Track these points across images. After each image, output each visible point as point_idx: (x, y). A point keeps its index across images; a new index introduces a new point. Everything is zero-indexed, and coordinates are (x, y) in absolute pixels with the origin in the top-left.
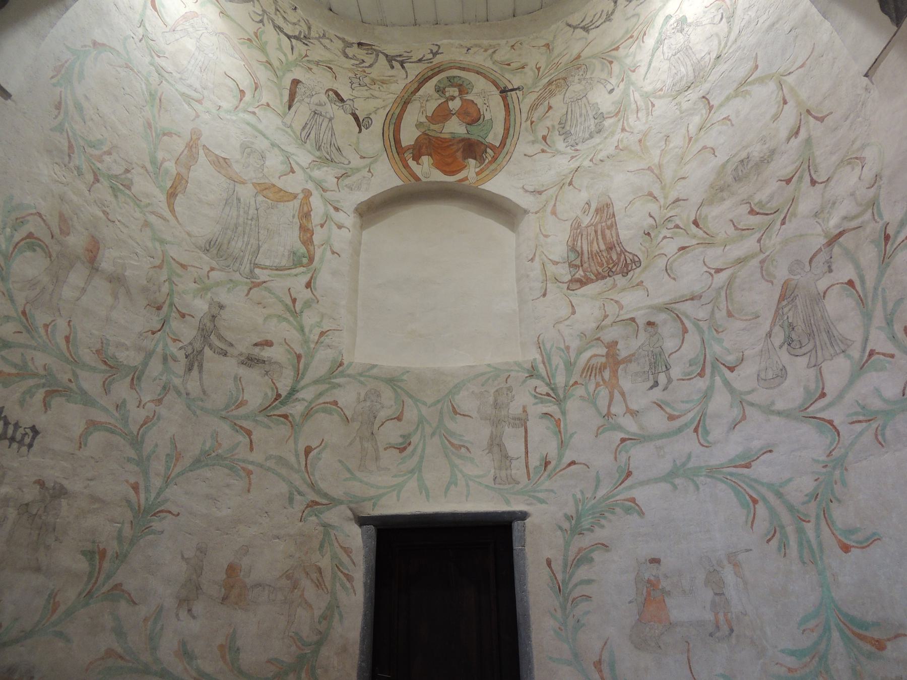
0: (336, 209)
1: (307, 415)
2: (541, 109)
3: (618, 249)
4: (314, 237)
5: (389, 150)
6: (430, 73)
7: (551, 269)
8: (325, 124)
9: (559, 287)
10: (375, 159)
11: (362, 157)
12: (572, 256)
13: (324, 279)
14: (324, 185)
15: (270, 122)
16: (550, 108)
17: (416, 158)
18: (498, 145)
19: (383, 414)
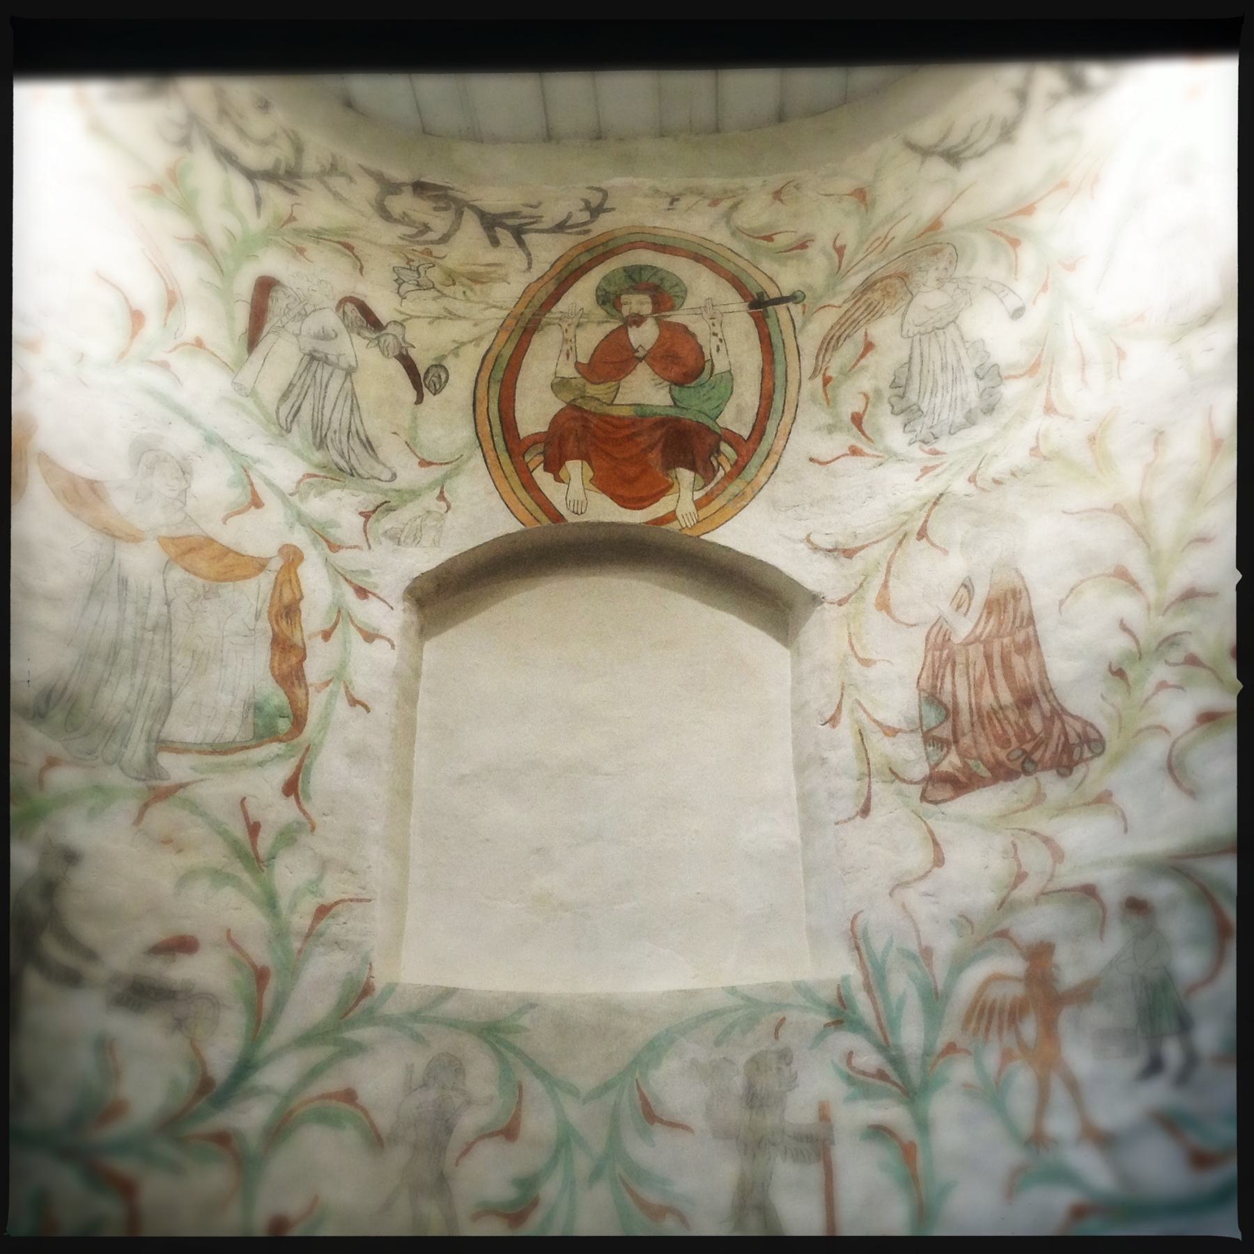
0: (362, 592)
1: (279, 1130)
2: (848, 351)
3: (1046, 706)
4: (307, 664)
5: (488, 445)
6: (585, 259)
7: (881, 746)
8: (335, 385)
9: (900, 793)
10: (454, 466)
11: (424, 463)
12: (932, 717)
13: (331, 770)
14: (337, 534)
15: (204, 386)
16: (869, 346)
17: (554, 466)
18: (745, 433)
19: (469, 1122)
